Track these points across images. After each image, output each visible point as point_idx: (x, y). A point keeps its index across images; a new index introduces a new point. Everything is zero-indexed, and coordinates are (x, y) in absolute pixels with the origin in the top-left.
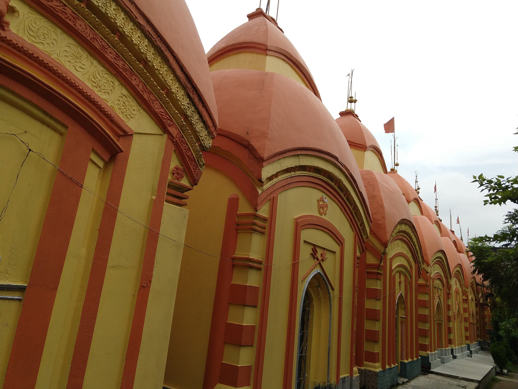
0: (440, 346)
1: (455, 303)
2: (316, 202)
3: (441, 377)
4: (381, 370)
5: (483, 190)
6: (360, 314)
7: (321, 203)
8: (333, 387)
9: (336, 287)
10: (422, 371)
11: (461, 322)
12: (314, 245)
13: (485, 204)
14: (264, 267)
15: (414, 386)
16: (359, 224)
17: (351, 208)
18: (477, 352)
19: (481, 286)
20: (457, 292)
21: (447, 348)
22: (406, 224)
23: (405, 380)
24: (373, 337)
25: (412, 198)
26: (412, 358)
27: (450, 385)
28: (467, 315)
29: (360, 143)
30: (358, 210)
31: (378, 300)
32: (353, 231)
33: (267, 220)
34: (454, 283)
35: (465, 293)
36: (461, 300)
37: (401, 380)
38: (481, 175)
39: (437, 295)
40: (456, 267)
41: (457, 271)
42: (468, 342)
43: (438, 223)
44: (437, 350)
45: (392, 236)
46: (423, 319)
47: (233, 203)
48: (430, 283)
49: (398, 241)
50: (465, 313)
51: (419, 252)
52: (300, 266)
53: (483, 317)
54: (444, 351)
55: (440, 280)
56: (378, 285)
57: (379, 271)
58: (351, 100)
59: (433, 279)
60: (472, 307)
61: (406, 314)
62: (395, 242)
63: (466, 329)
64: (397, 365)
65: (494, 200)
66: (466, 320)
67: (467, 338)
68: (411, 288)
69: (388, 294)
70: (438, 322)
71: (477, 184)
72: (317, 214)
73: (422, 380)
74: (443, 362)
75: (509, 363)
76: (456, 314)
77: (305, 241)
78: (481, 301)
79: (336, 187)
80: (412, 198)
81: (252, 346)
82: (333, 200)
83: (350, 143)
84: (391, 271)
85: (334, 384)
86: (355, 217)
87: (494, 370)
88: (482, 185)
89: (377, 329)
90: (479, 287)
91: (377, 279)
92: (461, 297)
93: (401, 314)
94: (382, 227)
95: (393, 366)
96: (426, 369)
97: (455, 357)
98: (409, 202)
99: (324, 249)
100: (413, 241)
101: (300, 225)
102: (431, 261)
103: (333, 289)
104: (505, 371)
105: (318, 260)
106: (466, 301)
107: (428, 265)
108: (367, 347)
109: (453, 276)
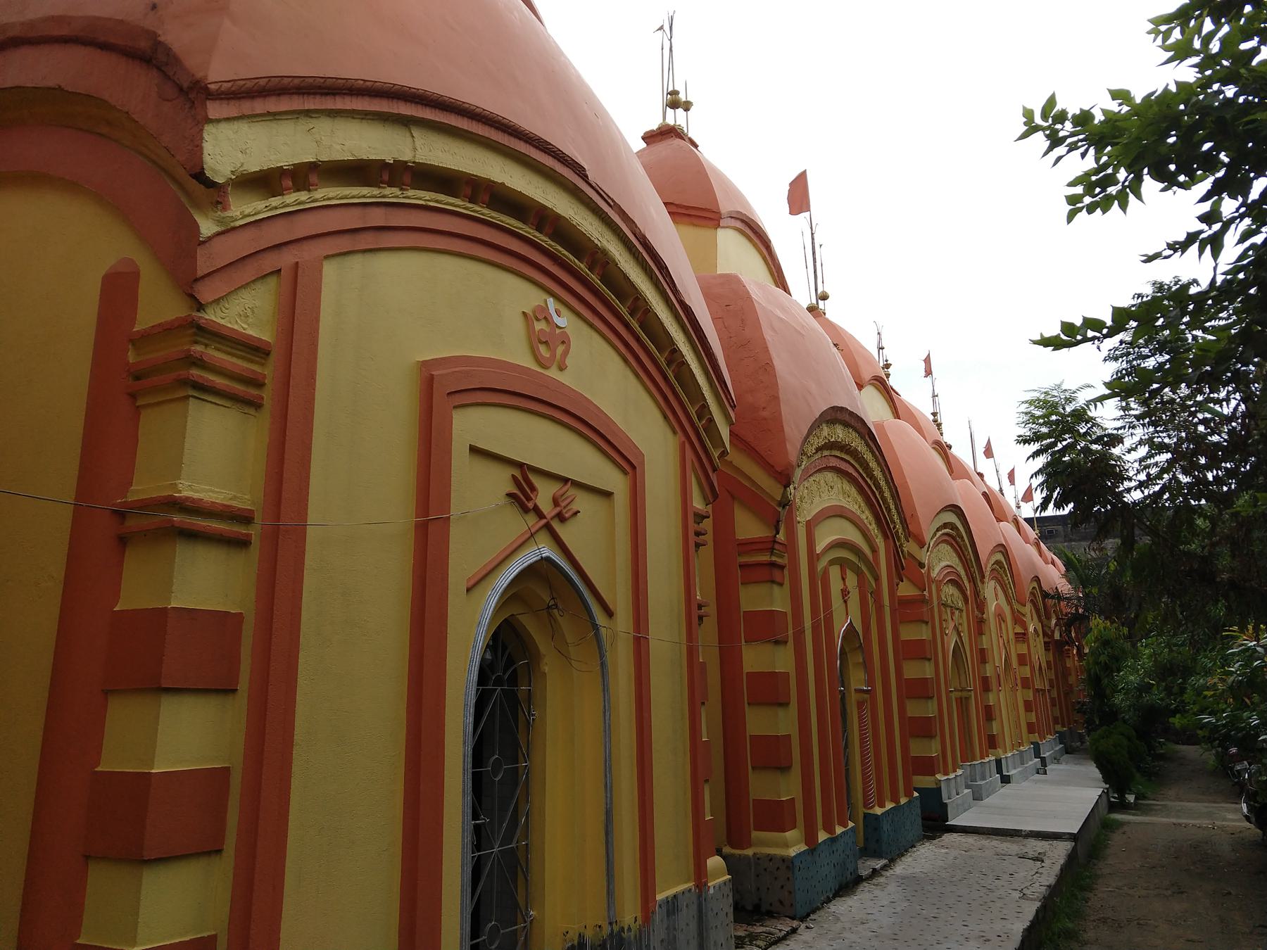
0: (967, 756)
1: (998, 642)
2: (519, 324)
3: (976, 837)
4: (803, 848)
5: (1059, 158)
6: (727, 689)
7: (540, 326)
8: (629, 936)
9: (621, 601)
10: (926, 828)
11: (1014, 689)
12: (521, 465)
13: (1071, 216)
14: (269, 532)
15: (904, 878)
16: (693, 411)
17: (662, 360)
18: (1057, 760)
19: (1053, 597)
20: (1000, 616)
21: (987, 760)
22: (846, 425)
23: (883, 862)
24: (772, 755)
25: (867, 375)
26: (895, 799)
27: (1001, 856)
28: (1026, 671)
29: (700, 205)
30: (684, 363)
31: (777, 642)
32: (675, 432)
33: (268, 354)
34: (990, 590)
35: (1018, 619)
36: (1011, 636)
37: (866, 866)
38: (1051, 101)
39: (951, 625)
40: (993, 552)
41: (998, 562)
42: (1035, 737)
43: (943, 449)
44: (961, 767)
45: (803, 453)
46: (920, 689)
47: (119, 289)
48: (930, 593)
49: (830, 476)
50: (1022, 668)
51: (892, 507)
52: (456, 533)
53: (1065, 673)
54: (978, 768)
55: (956, 583)
56: (777, 600)
57: (774, 558)
58: (674, 101)
59: (939, 583)
60: (1038, 652)
61: (870, 681)
62: (818, 477)
63: (1028, 706)
64: (851, 824)
65: (1096, 194)
66: (1026, 683)
67: (1031, 728)
68: (879, 607)
69: (808, 623)
70: (959, 694)
71: (1039, 141)
72: (527, 362)
73: (926, 857)
74: (977, 797)
75: (1138, 775)
76: (1001, 671)
77: (474, 450)
78: (1057, 636)
79: (595, 279)
80: (867, 375)
81: (219, 851)
82: (591, 326)
83: (674, 209)
84: (813, 557)
85: (634, 927)
86: (679, 389)
87: (1104, 797)
88: (1055, 141)
89: (782, 732)
90: (1050, 602)
91: (773, 582)
92: (1011, 629)
93: (857, 680)
94: (773, 425)
95: (839, 830)
96: (935, 821)
97: (1006, 780)
98: (860, 387)
99: (566, 480)
100: (872, 477)
101: (443, 391)
102: (928, 532)
103: (610, 613)
104: (1131, 798)
105: (541, 515)
106: (1022, 637)
107: (922, 544)
108: (761, 787)
109: (987, 574)
